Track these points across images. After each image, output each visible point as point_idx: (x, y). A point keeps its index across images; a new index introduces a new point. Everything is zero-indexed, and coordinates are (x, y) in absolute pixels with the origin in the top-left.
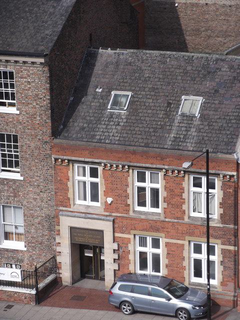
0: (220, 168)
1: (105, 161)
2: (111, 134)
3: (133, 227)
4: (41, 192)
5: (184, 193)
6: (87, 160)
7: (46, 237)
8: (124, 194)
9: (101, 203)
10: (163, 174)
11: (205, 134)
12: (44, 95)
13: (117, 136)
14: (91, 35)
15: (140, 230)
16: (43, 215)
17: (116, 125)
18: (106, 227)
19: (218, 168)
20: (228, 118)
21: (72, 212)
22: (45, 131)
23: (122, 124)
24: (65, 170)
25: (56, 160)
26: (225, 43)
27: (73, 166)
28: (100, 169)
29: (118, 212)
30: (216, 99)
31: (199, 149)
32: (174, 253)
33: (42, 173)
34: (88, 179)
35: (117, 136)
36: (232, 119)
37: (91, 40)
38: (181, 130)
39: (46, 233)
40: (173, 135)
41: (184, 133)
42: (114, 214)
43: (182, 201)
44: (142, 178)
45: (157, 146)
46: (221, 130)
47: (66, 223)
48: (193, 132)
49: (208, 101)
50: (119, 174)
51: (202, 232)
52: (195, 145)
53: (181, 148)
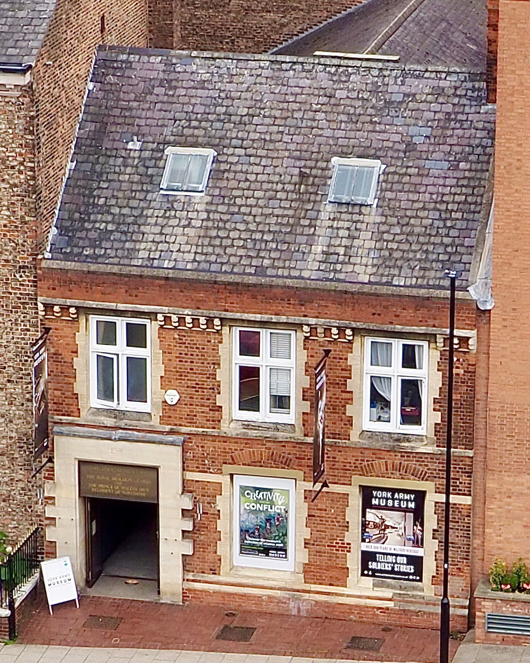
0: (437, 323)
1: (166, 309)
2: (175, 247)
3: (228, 457)
4: (9, 381)
5: (350, 378)
6: (121, 307)
7: (21, 485)
8: (209, 383)
9: (153, 404)
10: (301, 336)
11: (394, 246)
12: (20, 159)
13: (189, 252)
14: (103, 17)
15: (244, 464)
16: (14, 435)
17: (184, 227)
18: (167, 460)
19: (431, 322)
20: (443, 207)
21: (83, 426)
22: (21, 241)
23: (198, 224)
24: (68, 331)
25: (48, 307)
26: (283, 25)
27: (87, 320)
28: (152, 329)
29: (192, 423)
30: (411, 164)
31: (384, 280)
32: (323, 514)
33: (13, 338)
34: (121, 350)
35: (189, 252)
36: (452, 210)
37: (103, 30)
38: (337, 236)
39: (20, 474)
40: (319, 249)
41: (345, 242)
42: (184, 430)
43: (344, 395)
44: (249, 346)
45: (286, 274)
46: (430, 235)
47: (70, 450)
48: (366, 240)
49: (392, 169)
50: (198, 339)
51: (390, 466)
52: (375, 270)
53: (342, 276)
